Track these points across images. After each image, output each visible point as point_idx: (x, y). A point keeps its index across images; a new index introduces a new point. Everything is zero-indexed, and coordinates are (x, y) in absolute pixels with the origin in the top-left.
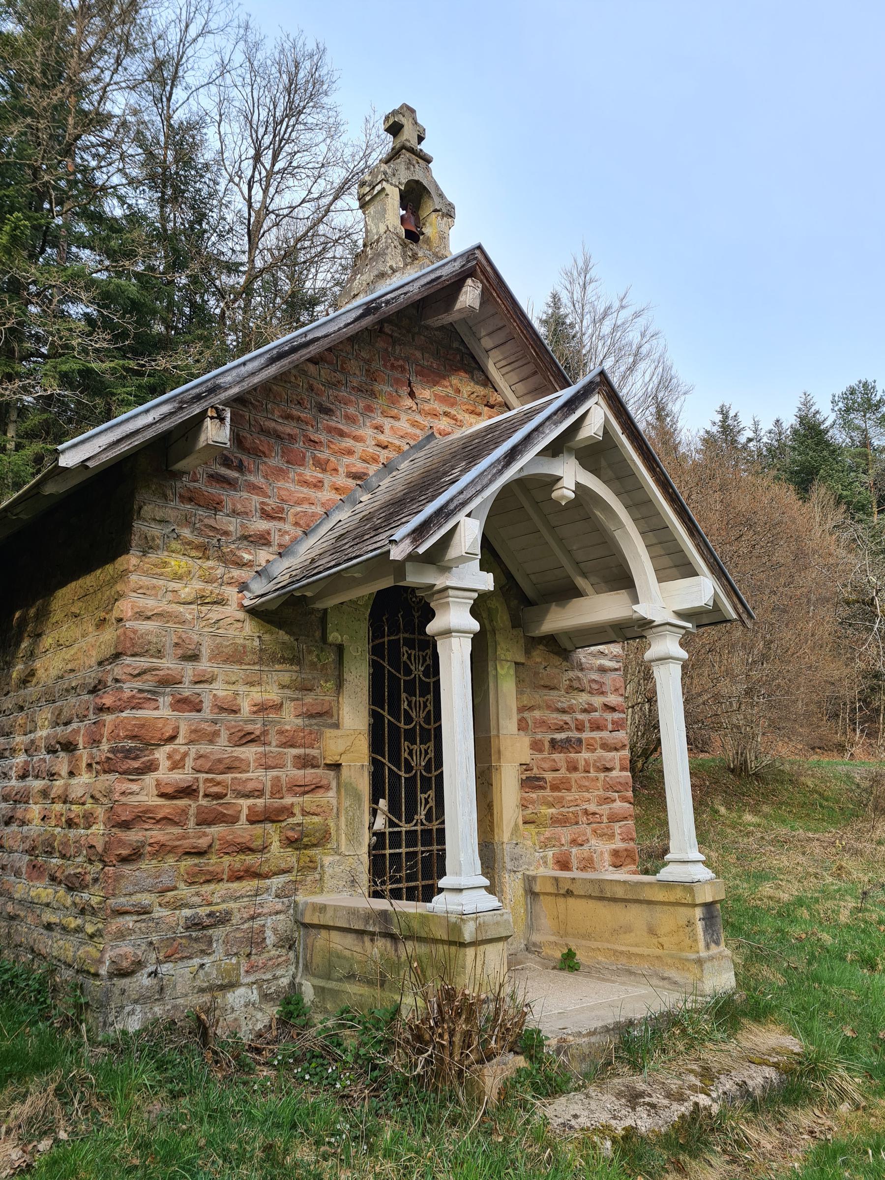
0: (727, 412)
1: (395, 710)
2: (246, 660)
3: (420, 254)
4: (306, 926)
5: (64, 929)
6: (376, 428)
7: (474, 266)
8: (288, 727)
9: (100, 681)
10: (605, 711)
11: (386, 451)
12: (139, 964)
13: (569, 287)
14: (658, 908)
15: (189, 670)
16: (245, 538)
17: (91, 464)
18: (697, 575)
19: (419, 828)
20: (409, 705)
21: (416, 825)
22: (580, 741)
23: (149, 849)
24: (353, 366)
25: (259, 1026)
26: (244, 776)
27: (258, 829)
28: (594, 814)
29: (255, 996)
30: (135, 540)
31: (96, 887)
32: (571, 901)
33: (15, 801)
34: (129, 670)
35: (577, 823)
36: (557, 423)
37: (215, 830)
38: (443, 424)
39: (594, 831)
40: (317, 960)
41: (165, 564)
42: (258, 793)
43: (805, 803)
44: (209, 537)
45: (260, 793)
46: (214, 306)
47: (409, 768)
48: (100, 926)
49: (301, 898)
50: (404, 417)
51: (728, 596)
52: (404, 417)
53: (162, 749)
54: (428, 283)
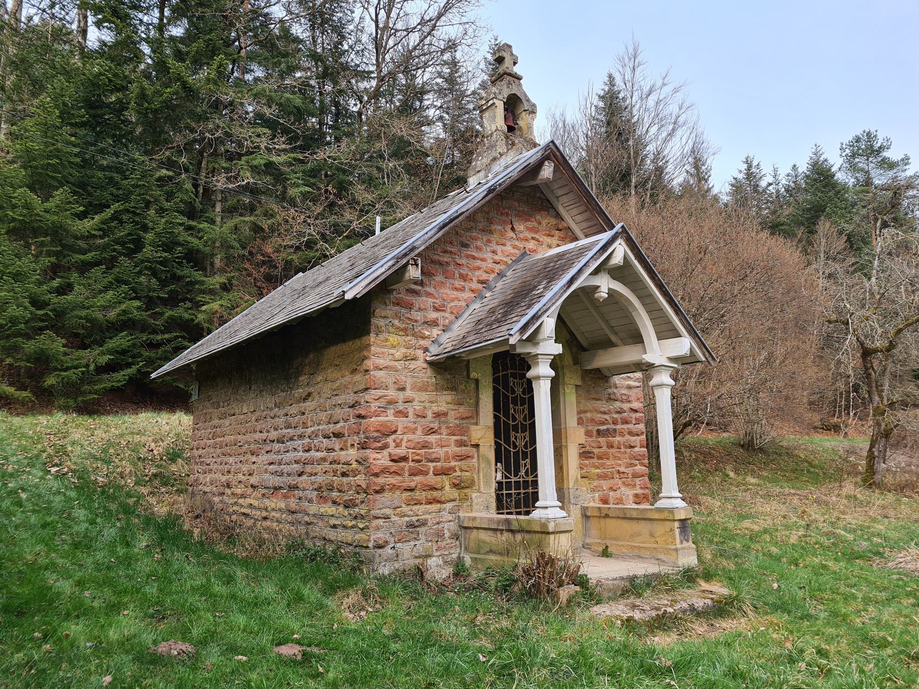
0: (751, 162)
1: (506, 415)
3: (516, 142)
4: (466, 528)
5: (345, 527)
6: (493, 252)
7: (549, 153)
8: (451, 425)
9: (356, 402)
10: (631, 412)
12: (387, 542)
13: (621, 70)
14: (656, 522)
15: (401, 396)
16: (425, 323)
18: (681, 336)
19: (521, 480)
20: (514, 411)
22: (615, 430)
25: (444, 576)
27: (439, 478)
28: (623, 473)
29: (441, 562)
30: (373, 327)
31: (363, 505)
32: (608, 520)
33: (304, 464)
34: (373, 397)
35: (613, 478)
38: (531, 245)
39: (624, 483)
40: (472, 545)
41: (387, 340)
42: (437, 460)
43: (796, 470)
44: (408, 324)
46: (354, 106)
47: (515, 446)
48: (367, 524)
49: (461, 514)
50: (509, 243)
51: (700, 348)
52: (509, 243)
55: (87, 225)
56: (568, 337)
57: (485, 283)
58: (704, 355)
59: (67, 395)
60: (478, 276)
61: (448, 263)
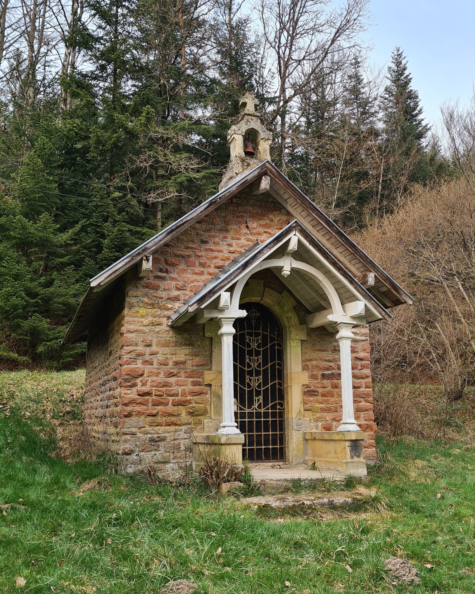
2: (171, 345)
3: (251, 163)
6: (229, 245)
7: (266, 170)
8: (188, 370)
10: (356, 360)
11: (234, 254)
15: (148, 350)
16: (169, 299)
17: (101, 284)
19: (254, 411)
20: (250, 360)
21: (253, 410)
23: (135, 413)
24: (218, 220)
26: (171, 388)
27: (176, 408)
30: (126, 304)
34: (125, 351)
35: (336, 411)
36: (270, 248)
37: (159, 408)
41: (138, 312)
44: (154, 300)
45: (177, 395)
47: (249, 386)
53: (139, 379)
54: (241, 185)
55: (64, 237)
56: (295, 304)
57: (220, 268)
58: (381, 314)
59: (51, 358)
60: (215, 264)
61: (189, 256)
